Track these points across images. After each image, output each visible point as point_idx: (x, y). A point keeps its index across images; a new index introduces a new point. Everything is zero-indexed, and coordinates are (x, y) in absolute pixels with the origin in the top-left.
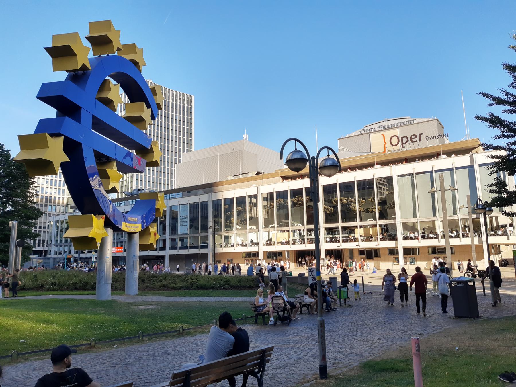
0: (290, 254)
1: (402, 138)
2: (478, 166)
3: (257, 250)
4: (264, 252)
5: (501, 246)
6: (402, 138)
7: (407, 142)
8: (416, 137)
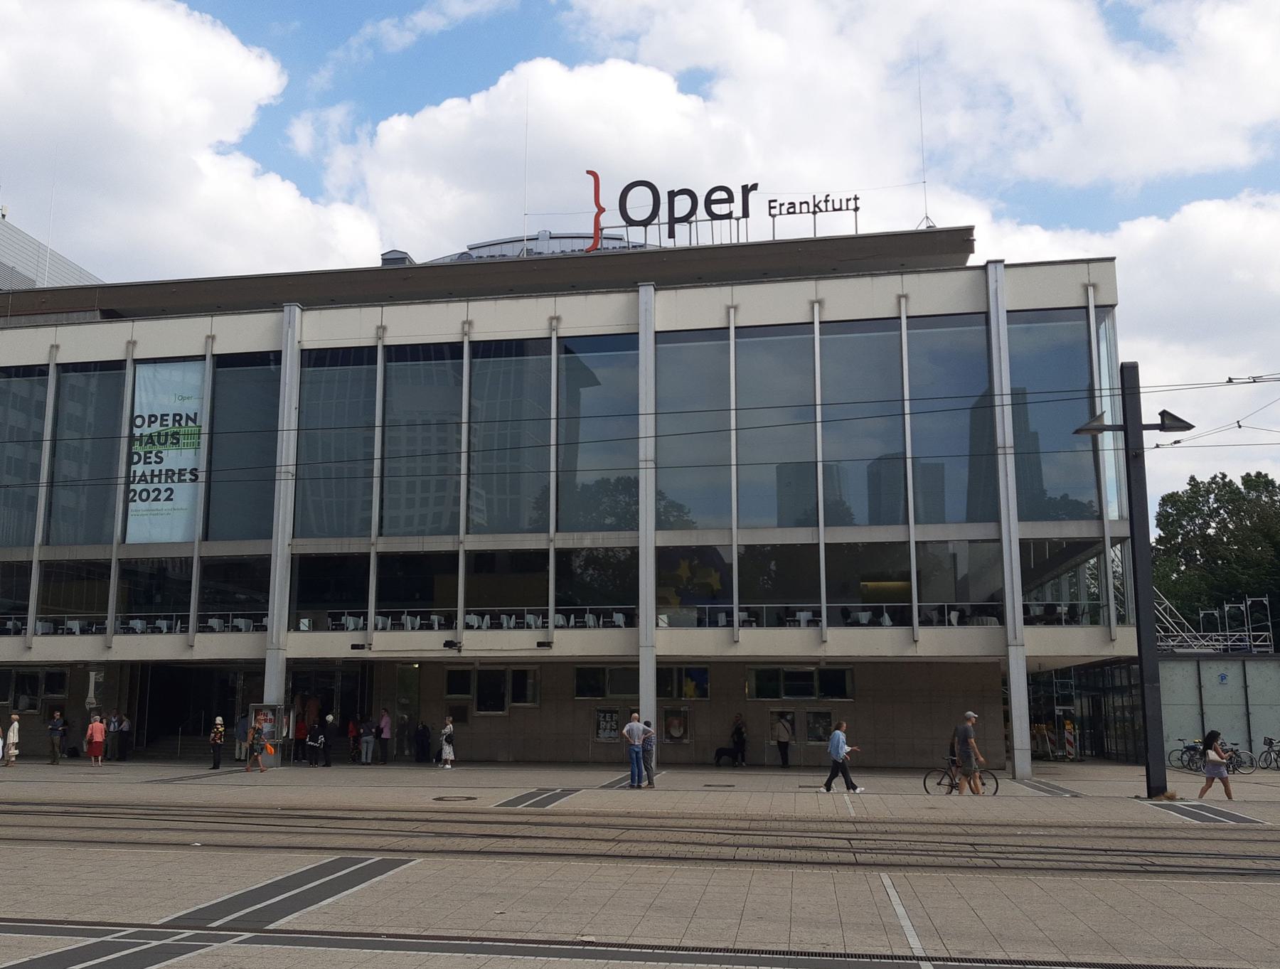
0: (901, 517)
1: (672, 195)
2: (1003, 317)
5: (1145, 794)
6: (672, 195)
7: (645, 223)
8: (730, 200)
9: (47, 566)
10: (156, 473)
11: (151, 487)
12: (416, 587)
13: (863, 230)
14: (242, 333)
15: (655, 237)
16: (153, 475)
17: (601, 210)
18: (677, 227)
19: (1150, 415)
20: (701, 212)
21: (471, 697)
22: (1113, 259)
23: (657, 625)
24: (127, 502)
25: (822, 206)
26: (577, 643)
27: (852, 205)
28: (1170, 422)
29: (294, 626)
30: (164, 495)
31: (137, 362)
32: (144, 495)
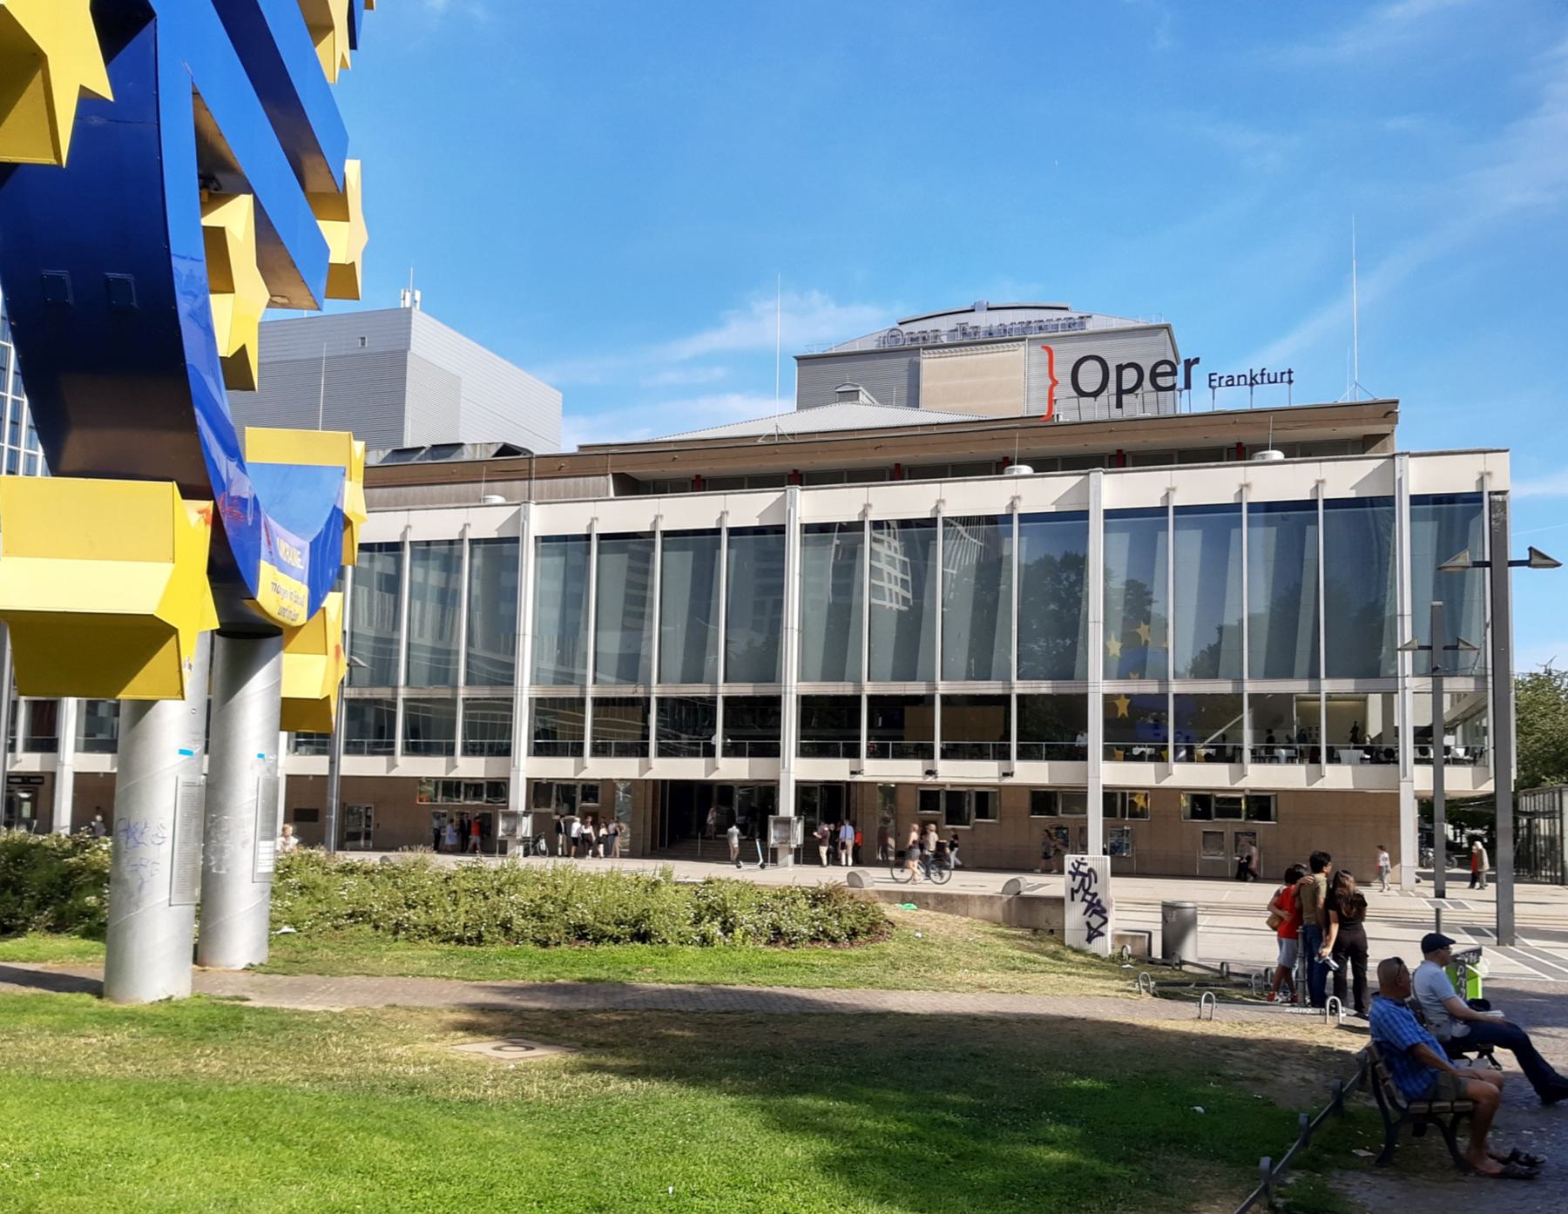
1: (1120, 368)
6: (1120, 368)
7: (1095, 394)
8: (1174, 373)
9: (599, 702)
12: (898, 725)
15: (1100, 409)
18: (1125, 398)
19: (1517, 551)
20: (1147, 383)
21: (941, 813)
25: (1259, 379)
26: (1034, 773)
27: (1286, 377)
28: (1537, 559)
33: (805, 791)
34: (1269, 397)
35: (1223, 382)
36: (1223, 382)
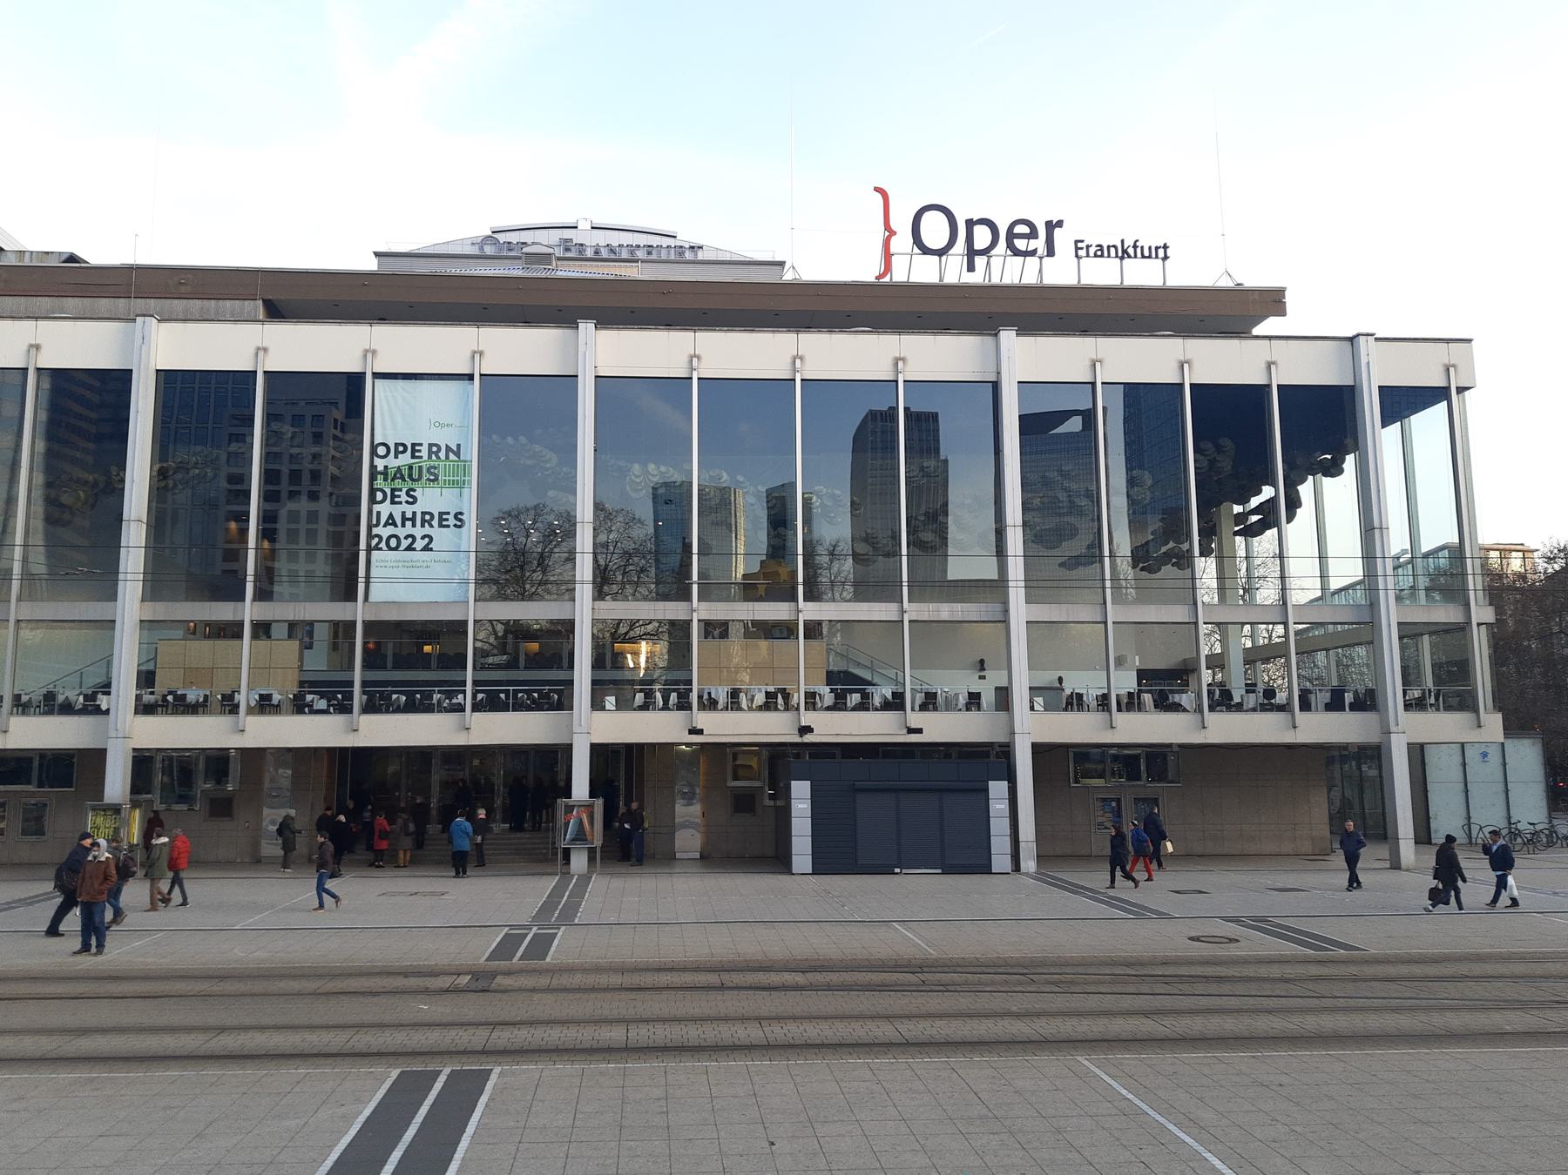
1: (970, 224)
3: (1372, 737)
4: (595, 748)
6: (970, 224)
7: (941, 253)
8: (1033, 234)
10: (409, 515)
11: (401, 532)
13: (1172, 282)
14: (78, 343)
15: (954, 271)
16: (404, 519)
17: (892, 233)
22: (1470, 341)
23: (1032, 708)
24: (369, 549)
25: (1131, 251)
27: (1161, 253)
29: (598, 705)
30: (419, 544)
31: (376, 375)
32: (393, 543)
33: (143, 761)
34: (1141, 274)
35: (1092, 251)
36: (1092, 251)
